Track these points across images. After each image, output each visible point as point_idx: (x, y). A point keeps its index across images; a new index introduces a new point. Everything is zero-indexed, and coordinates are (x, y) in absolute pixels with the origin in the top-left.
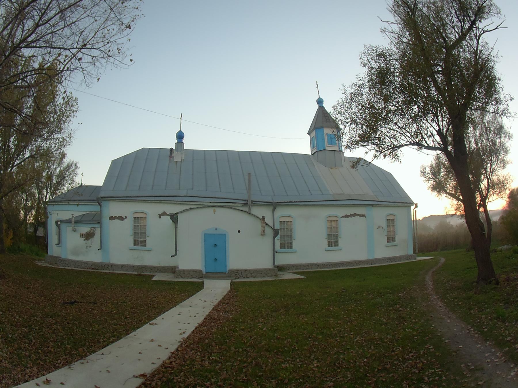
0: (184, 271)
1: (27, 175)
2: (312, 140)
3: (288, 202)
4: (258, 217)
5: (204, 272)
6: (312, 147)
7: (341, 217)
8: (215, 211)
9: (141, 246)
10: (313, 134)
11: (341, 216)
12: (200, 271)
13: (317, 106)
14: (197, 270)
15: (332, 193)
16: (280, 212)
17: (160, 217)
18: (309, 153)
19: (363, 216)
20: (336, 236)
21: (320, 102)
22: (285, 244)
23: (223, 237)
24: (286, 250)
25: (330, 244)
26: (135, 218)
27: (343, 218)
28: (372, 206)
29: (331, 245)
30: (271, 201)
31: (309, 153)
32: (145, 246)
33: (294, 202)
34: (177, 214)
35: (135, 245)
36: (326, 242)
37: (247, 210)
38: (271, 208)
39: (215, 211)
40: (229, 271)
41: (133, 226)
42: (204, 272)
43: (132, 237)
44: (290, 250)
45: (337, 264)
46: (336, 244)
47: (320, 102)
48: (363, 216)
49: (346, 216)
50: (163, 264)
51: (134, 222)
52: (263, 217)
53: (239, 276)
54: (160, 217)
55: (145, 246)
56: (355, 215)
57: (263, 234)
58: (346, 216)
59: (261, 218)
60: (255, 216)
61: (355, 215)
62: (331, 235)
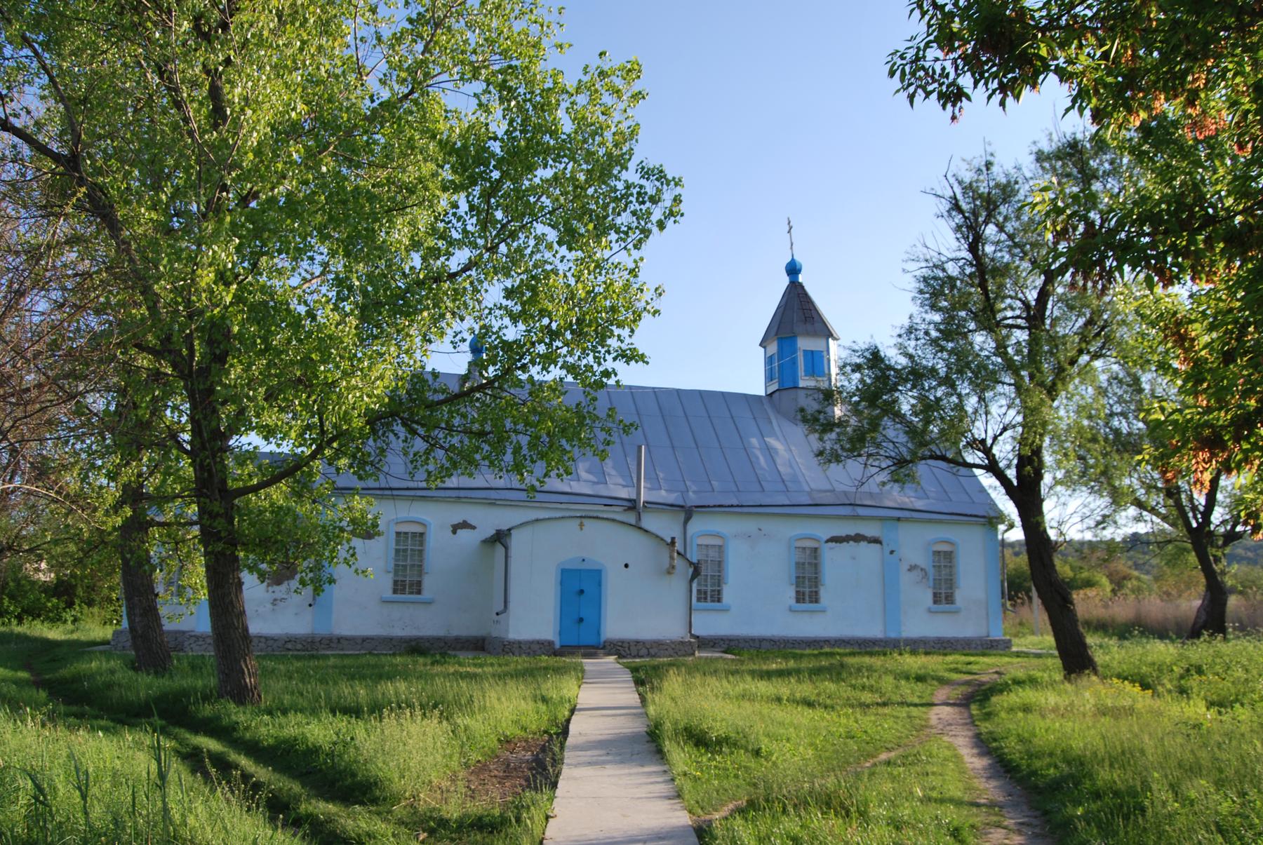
0: (520, 642)
1: (1255, 550)
2: (769, 360)
3: (715, 506)
4: (662, 539)
5: (557, 646)
6: (769, 377)
7: (827, 541)
8: (581, 525)
9: (411, 593)
10: (773, 348)
11: (828, 537)
12: (551, 643)
13: (785, 281)
14: (546, 641)
15: (807, 489)
16: (697, 525)
17: (454, 532)
18: (763, 393)
19: (876, 541)
20: (816, 581)
21: (793, 270)
22: (705, 593)
23: (596, 576)
24: (709, 605)
25: (800, 598)
26: (398, 534)
27: (831, 544)
28: (899, 519)
29: (804, 599)
30: (681, 503)
31: (761, 391)
32: (419, 592)
33: (729, 506)
34: (509, 530)
35: (395, 592)
36: (791, 593)
37: (633, 521)
38: (682, 516)
39: (581, 525)
40: (605, 642)
41: (393, 552)
42: (557, 646)
43: (391, 575)
44: (716, 605)
45: (815, 641)
46: (815, 598)
47: (793, 270)
48: (876, 541)
49: (835, 540)
50: (455, 632)
51: (398, 543)
52: (673, 539)
53: (623, 653)
54: (454, 532)
55: (419, 592)
56: (858, 538)
57: (671, 570)
58: (835, 540)
59: (669, 540)
60: (657, 536)
61: (858, 538)
62: (804, 577)
